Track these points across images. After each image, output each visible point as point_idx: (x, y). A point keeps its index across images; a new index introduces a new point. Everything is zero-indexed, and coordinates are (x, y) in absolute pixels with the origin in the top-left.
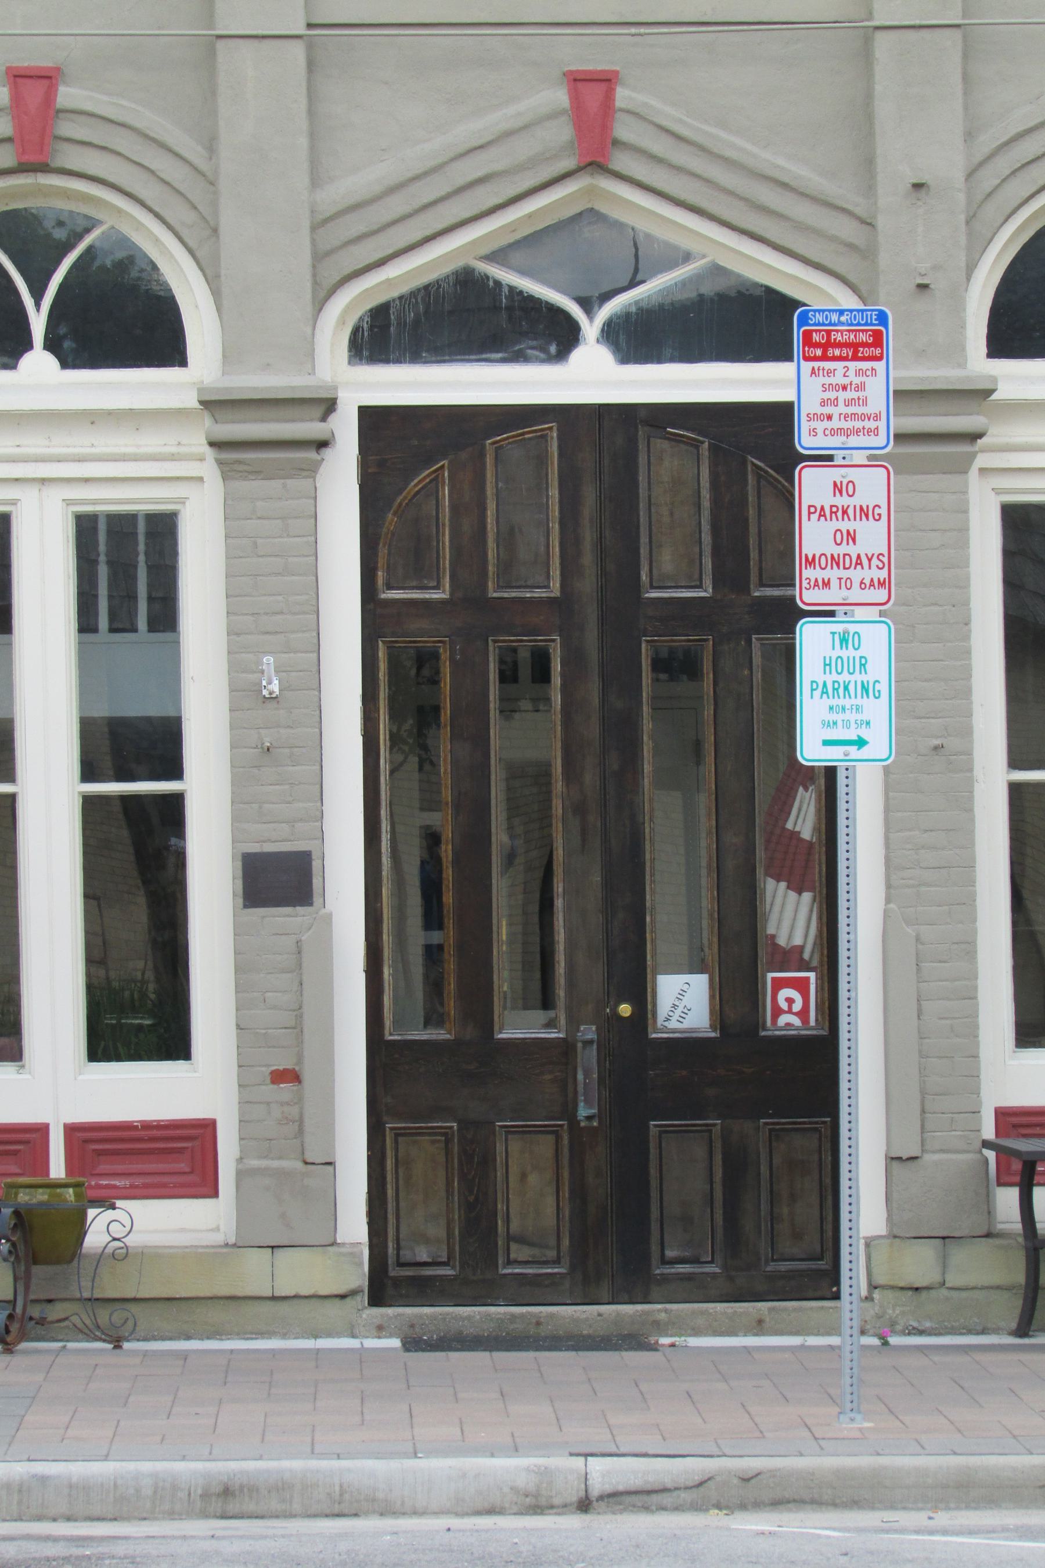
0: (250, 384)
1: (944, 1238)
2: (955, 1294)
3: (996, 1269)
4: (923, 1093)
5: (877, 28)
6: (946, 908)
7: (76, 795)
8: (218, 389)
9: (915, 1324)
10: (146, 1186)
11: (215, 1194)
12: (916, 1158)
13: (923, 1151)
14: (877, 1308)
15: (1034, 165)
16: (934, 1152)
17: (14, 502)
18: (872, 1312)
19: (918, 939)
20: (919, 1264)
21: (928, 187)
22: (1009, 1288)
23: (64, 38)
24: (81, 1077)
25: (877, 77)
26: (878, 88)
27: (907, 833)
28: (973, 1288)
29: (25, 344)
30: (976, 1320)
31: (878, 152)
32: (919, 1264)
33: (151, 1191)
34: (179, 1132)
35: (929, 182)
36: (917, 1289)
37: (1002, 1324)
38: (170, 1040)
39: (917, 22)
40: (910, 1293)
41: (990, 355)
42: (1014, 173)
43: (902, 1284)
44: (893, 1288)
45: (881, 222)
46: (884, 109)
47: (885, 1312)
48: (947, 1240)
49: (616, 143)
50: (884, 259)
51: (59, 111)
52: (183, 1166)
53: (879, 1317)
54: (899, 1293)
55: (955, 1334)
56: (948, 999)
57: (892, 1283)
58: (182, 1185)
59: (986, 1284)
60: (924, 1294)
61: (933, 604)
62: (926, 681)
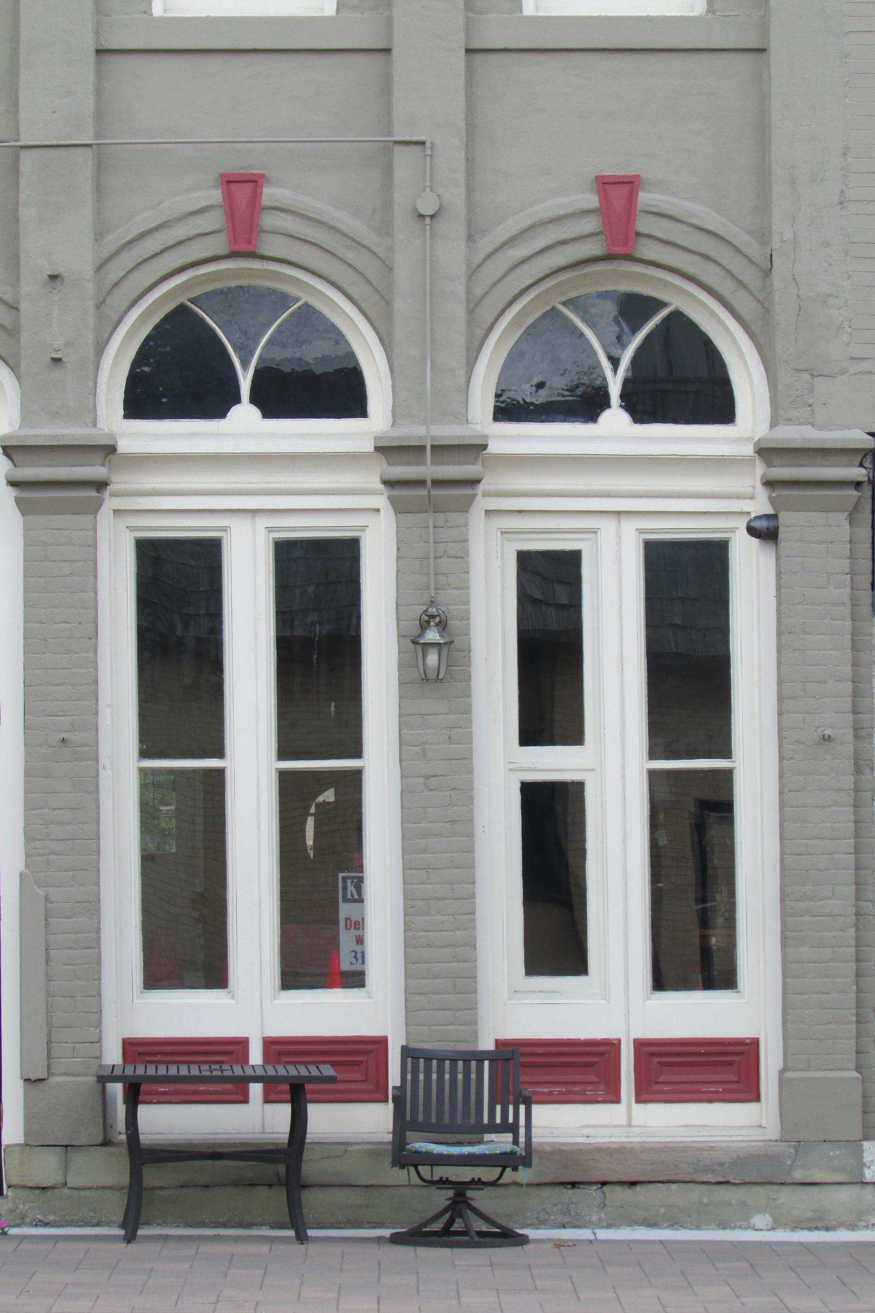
0: (458, 433)
1: (66, 1146)
2: (76, 1193)
3: (107, 1171)
4: (49, 1025)
5: (22, 147)
6: (71, 873)
7: (274, 770)
8: (18, 437)
9: (41, 1217)
10: (669, 1092)
11: (757, 1099)
12: (43, 1080)
13: (48, 1074)
14: (10, 1204)
15: (155, 260)
16: (58, 1075)
17: (225, 529)
18: (6, 1207)
19: (47, 898)
20: (45, 1168)
21: (62, 278)
22: (120, 1189)
23: (240, 145)
24: (276, 1002)
25: (21, 189)
26: (23, 197)
27: (38, 811)
28: (91, 1188)
29: (237, 400)
30: (92, 1214)
31: (21, 249)
32: (45, 1168)
33: (676, 1096)
34: (566, 1049)
35: (64, 274)
36: (44, 1188)
37: (114, 1218)
38: (213, 972)
39: (55, 142)
40: (38, 1192)
41: (127, 416)
42: (137, 266)
43: (30, 1184)
44: (23, 1187)
45: (23, 306)
46: (27, 214)
47: (17, 1208)
48: (69, 1148)
49: (638, 234)
50: (25, 337)
51: (264, 208)
52: (731, 1077)
53: (12, 1211)
54: (29, 1192)
55: (75, 1226)
56: (71, 948)
57: (22, 1183)
58: (725, 1091)
59: (101, 1185)
60: (49, 1193)
61: (62, 622)
62: (56, 685)
